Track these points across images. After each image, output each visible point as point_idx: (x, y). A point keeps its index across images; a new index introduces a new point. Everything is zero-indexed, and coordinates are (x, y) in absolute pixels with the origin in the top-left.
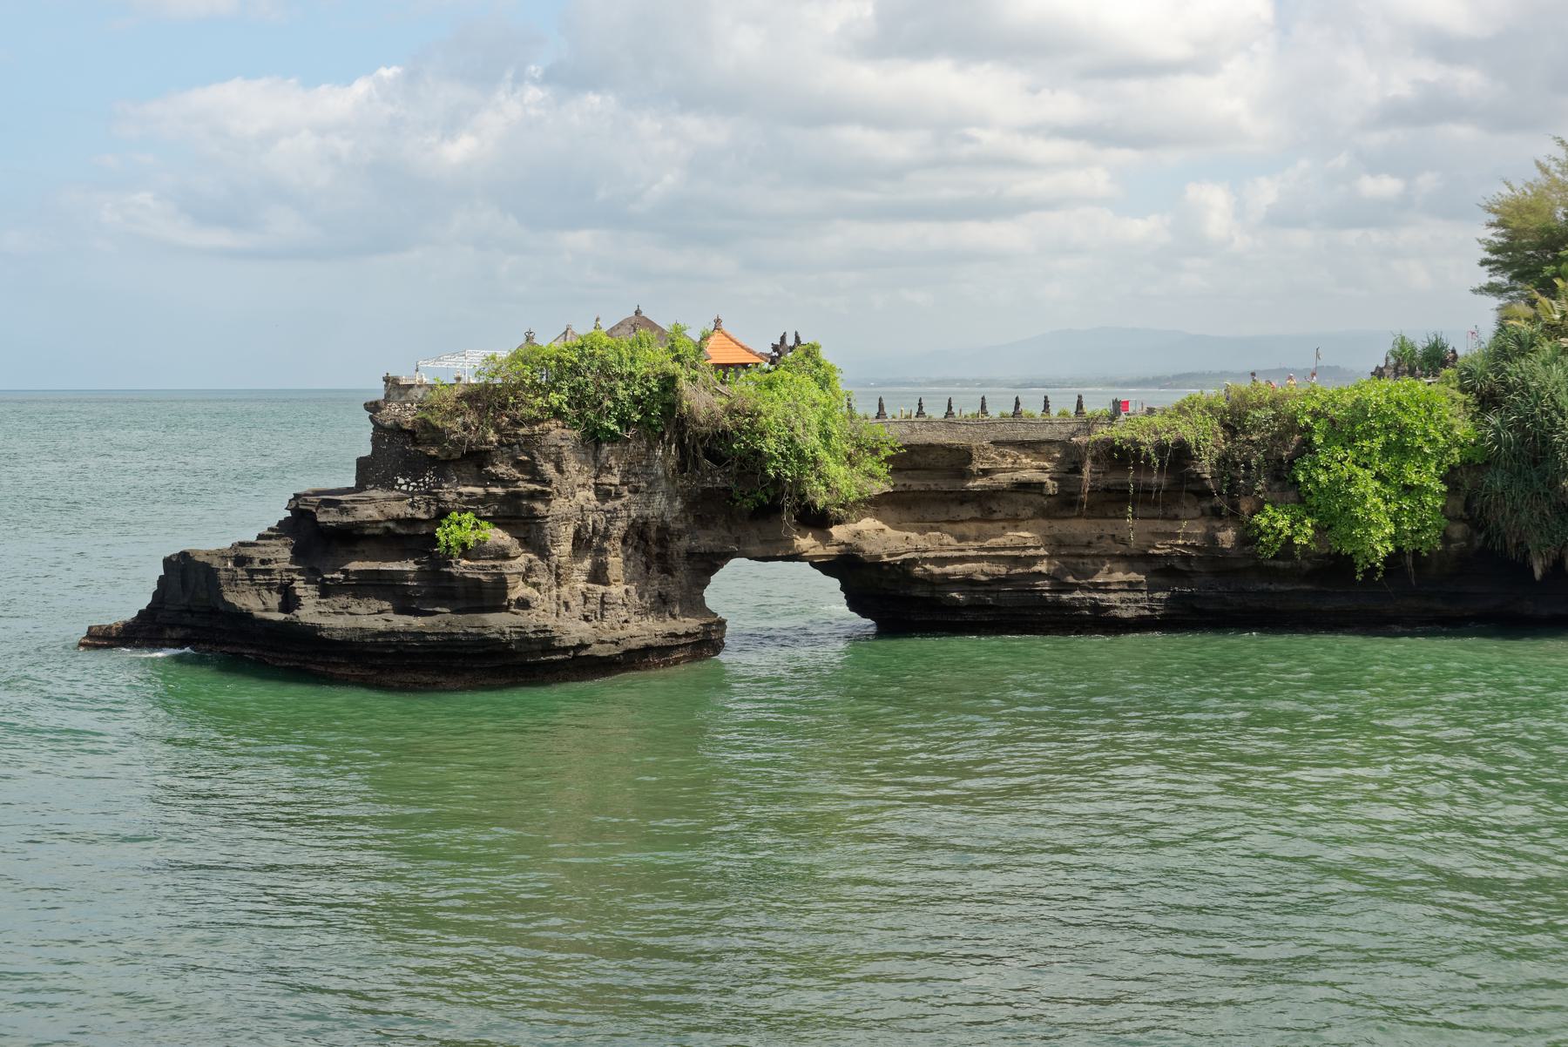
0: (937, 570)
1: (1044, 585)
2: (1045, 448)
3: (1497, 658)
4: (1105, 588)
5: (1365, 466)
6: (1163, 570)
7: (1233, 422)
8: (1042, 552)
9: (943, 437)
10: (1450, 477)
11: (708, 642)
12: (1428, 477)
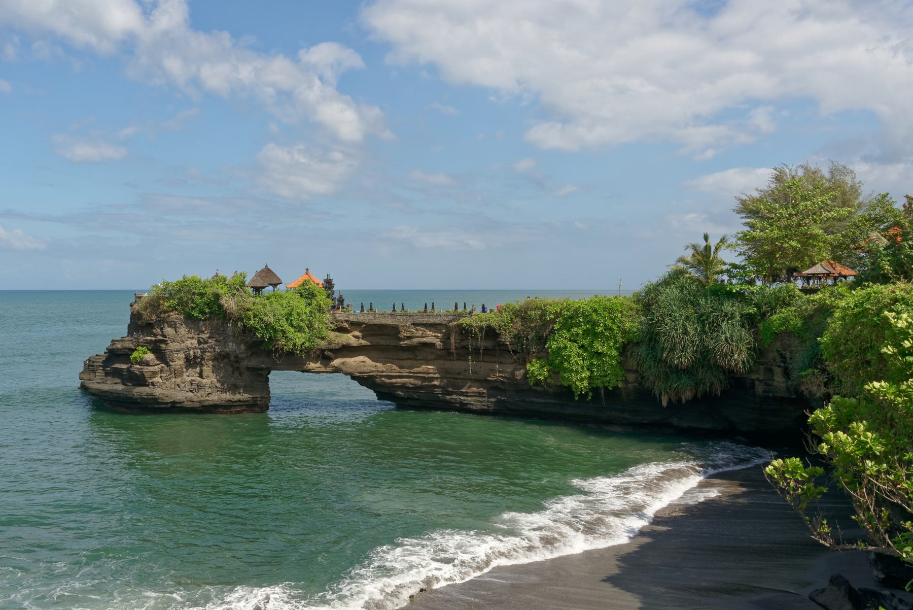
0: (387, 381)
1: (438, 391)
2: (439, 327)
3: (586, 452)
4: (466, 394)
5: (575, 341)
6: (494, 388)
7: (522, 314)
8: (437, 375)
9: (389, 321)
10: (623, 350)
11: (260, 406)
12: (608, 349)
